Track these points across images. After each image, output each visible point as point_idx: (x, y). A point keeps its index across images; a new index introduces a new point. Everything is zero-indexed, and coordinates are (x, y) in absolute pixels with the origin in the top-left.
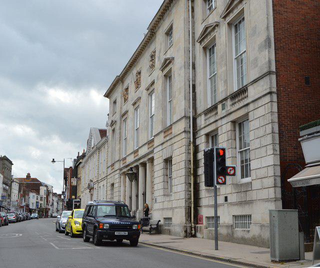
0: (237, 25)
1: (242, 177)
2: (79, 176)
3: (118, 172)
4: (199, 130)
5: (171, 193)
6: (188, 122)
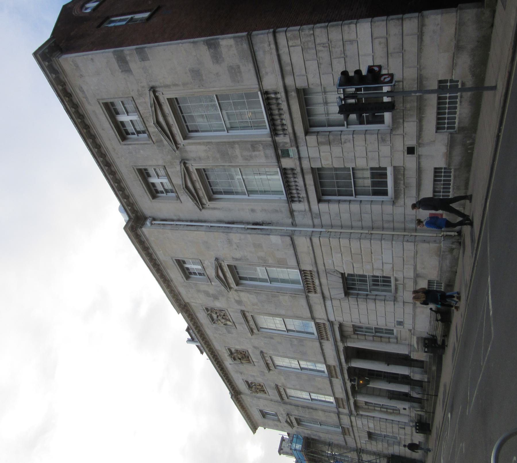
3: (353, 418)
5: (398, 438)
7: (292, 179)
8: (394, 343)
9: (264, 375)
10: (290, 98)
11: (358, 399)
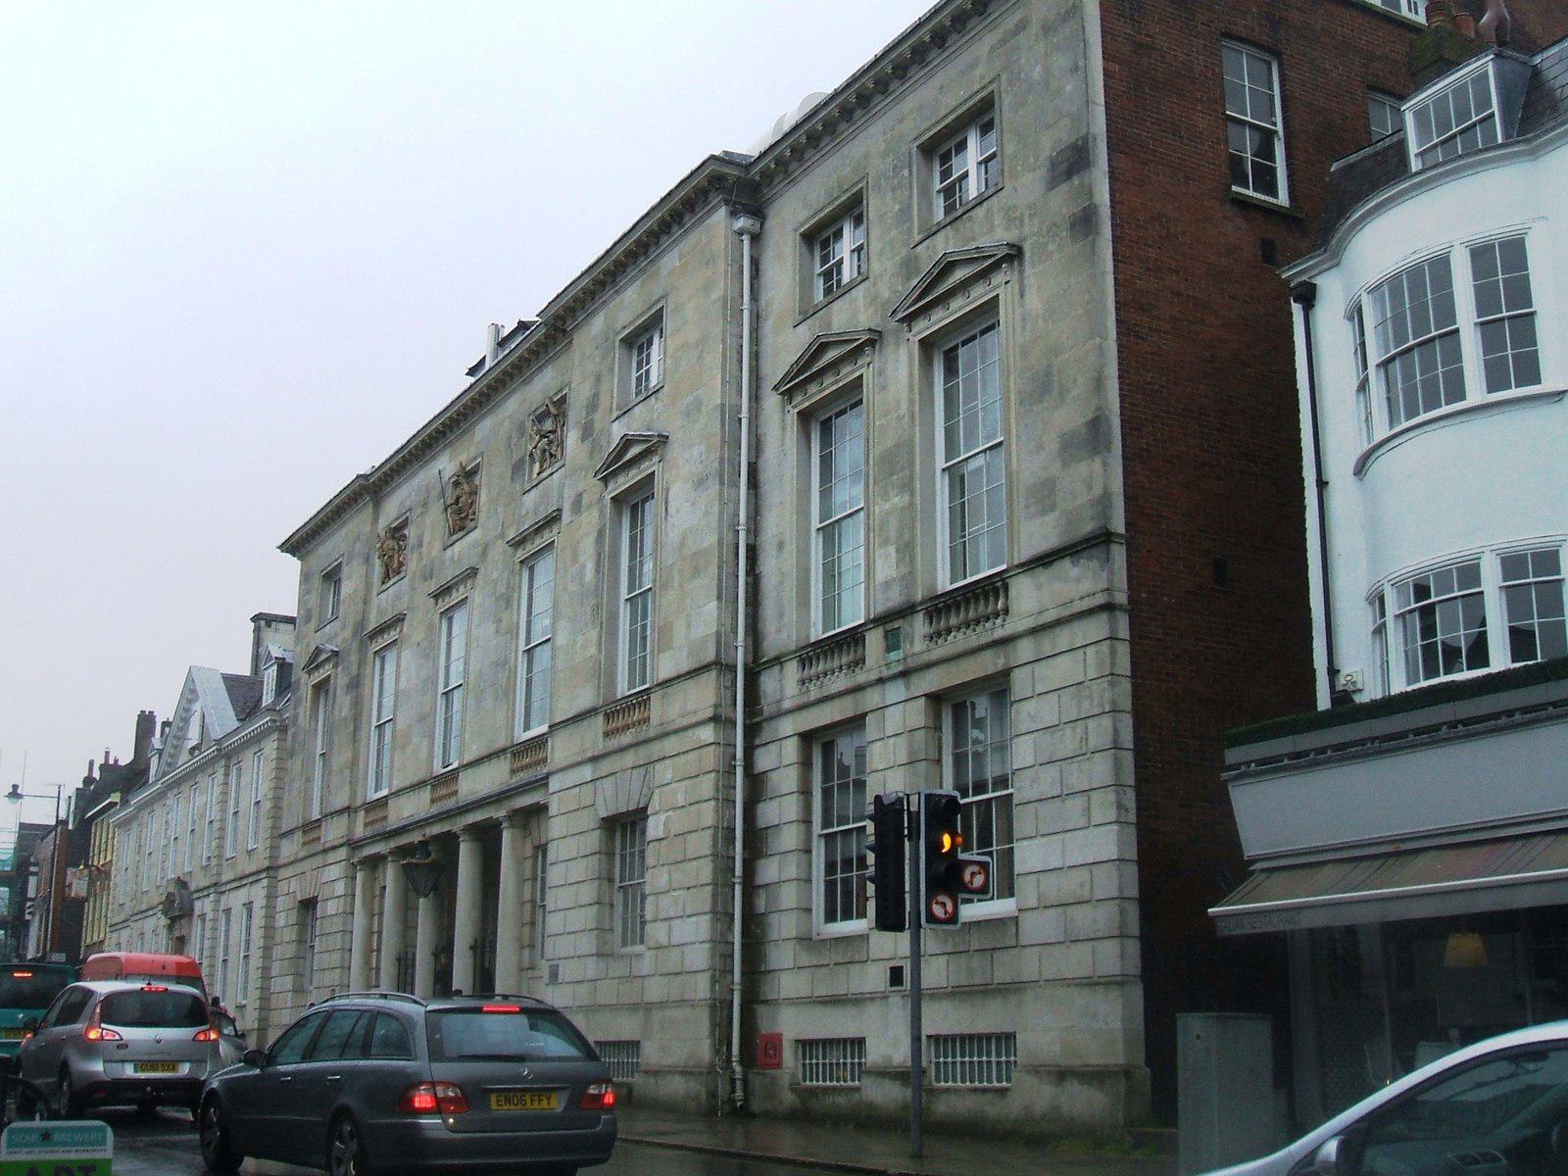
1: (831, 917)
2: (98, 861)
3: (343, 853)
4: (772, 718)
5: (311, 988)
6: (729, 684)
8: (520, 962)
11: (390, 865)
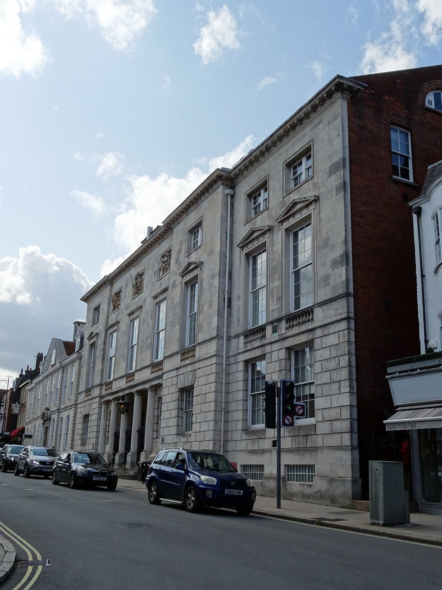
0: (256, 256)
5: (190, 432)
7: (259, 336)
9: (126, 309)
10: (308, 333)
